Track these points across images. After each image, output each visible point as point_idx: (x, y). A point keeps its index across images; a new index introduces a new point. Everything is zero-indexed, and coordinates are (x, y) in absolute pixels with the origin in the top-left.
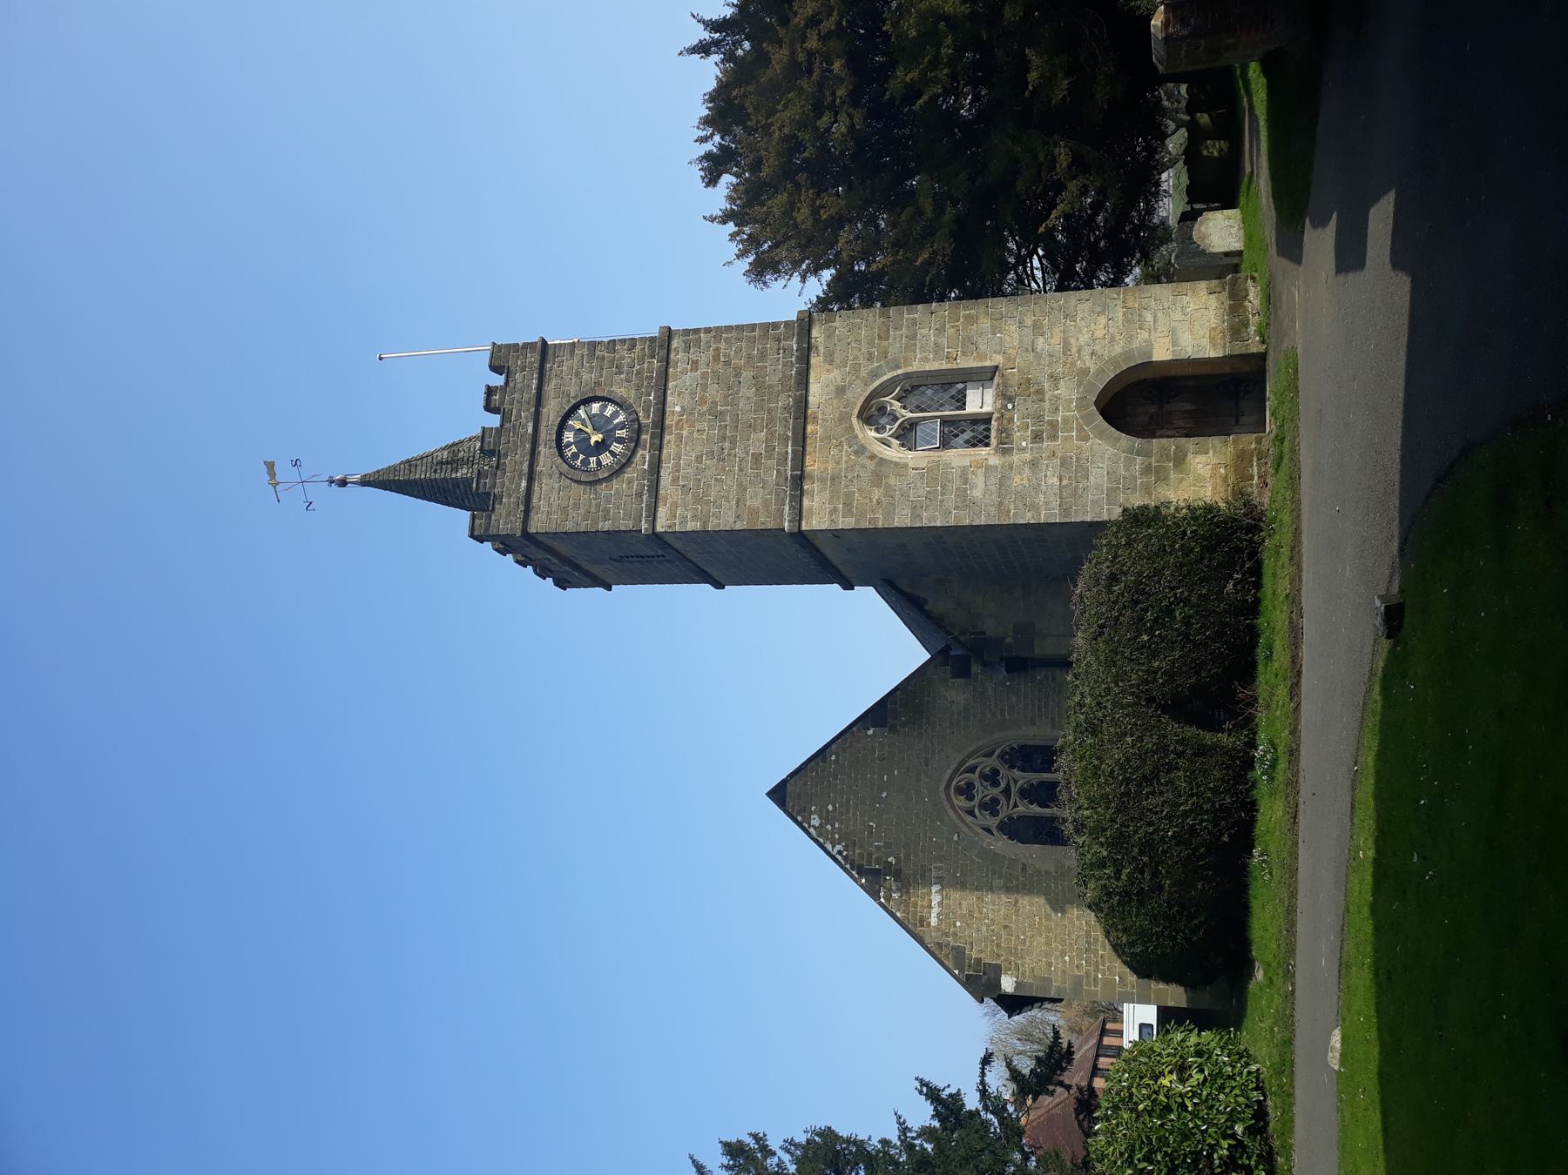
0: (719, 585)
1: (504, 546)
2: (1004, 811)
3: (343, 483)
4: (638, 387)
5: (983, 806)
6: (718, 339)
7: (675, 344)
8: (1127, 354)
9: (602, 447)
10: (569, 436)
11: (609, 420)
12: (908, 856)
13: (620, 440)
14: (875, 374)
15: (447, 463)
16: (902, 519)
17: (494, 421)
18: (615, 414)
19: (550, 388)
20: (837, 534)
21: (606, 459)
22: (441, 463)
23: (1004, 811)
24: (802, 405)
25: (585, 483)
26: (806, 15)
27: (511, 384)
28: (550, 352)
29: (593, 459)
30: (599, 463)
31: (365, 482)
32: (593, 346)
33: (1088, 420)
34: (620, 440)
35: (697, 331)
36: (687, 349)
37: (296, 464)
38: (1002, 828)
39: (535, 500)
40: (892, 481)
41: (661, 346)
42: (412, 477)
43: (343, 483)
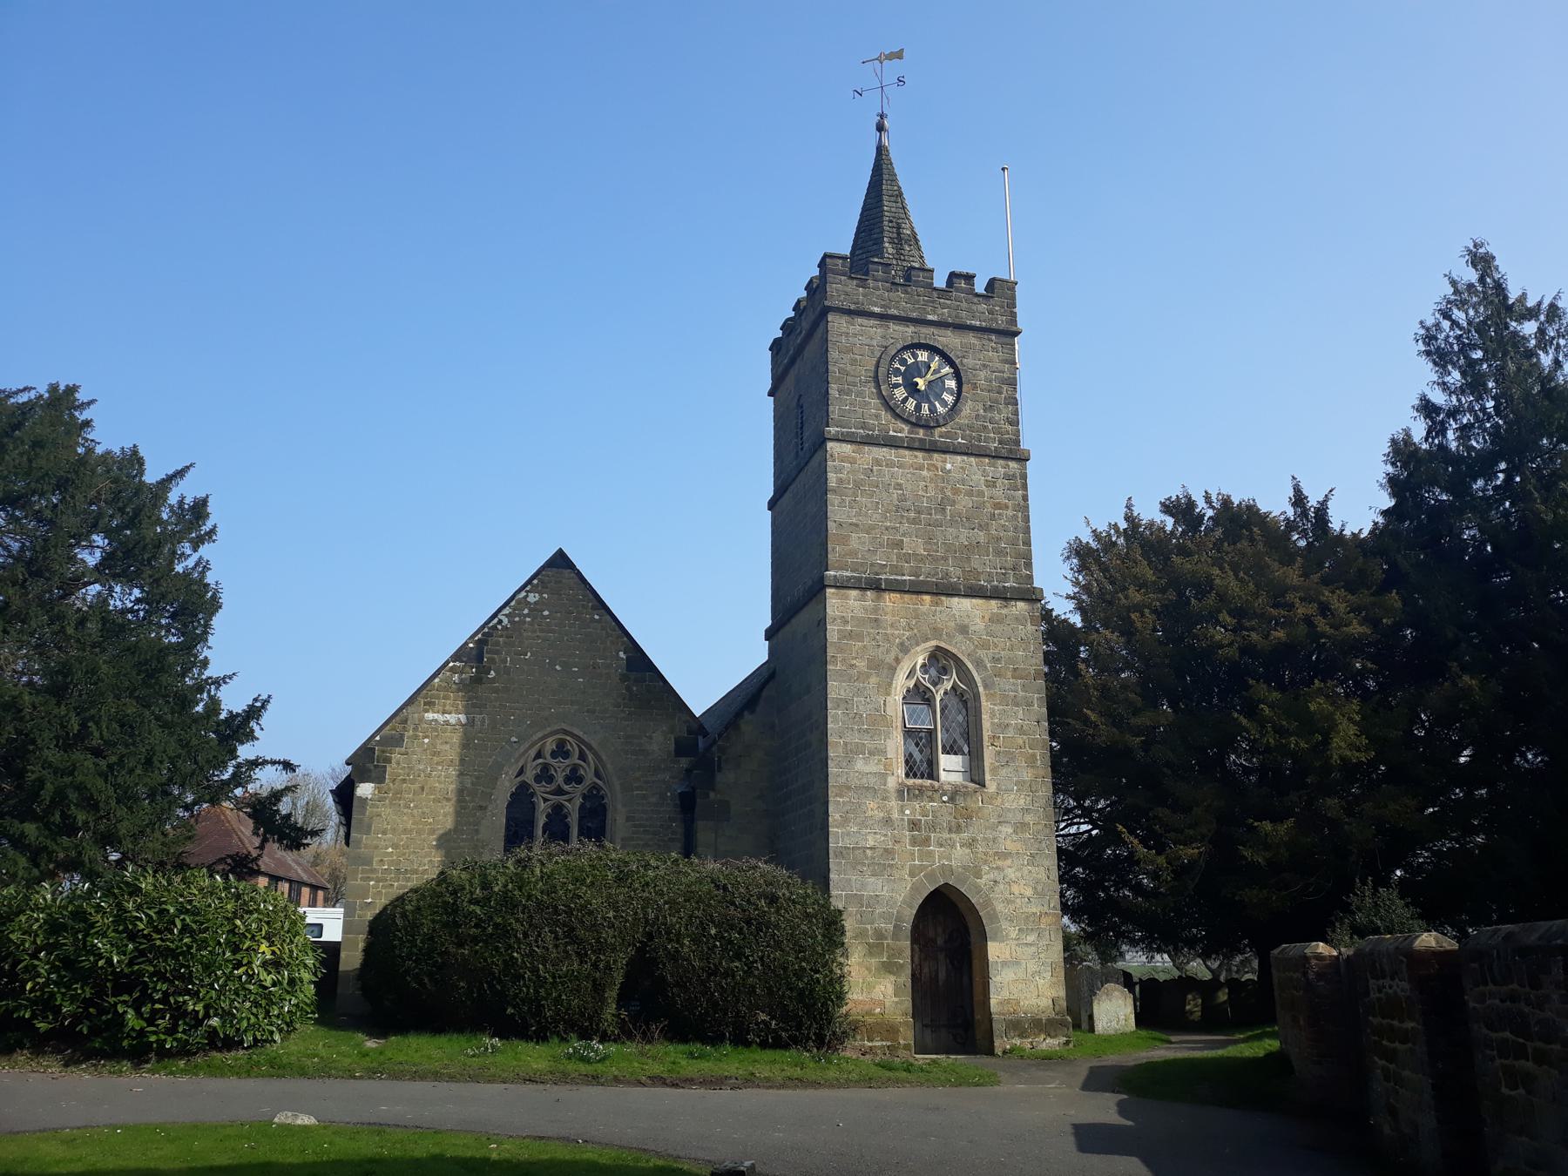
0: (772, 505)
1: (816, 289)
2: (539, 789)
3: (880, 128)
4: (971, 427)
5: (545, 767)
6: (1017, 508)
7: (1012, 464)
8: (994, 917)
9: (912, 389)
10: (923, 356)
11: (939, 397)
12: (496, 691)
13: (918, 408)
14: (979, 664)
15: (899, 234)
16: (835, 689)
17: (940, 281)
18: (944, 403)
19: (971, 339)
20: (822, 623)
21: (900, 393)
22: (899, 227)
23: (539, 789)
25: (876, 372)
27: (975, 300)
28: (1007, 340)
29: (900, 380)
30: (897, 386)
31: (881, 150)
32: (1012, 383)
33: (930, 876)
34: (918, 408)
35: (1025, 487)
36: (1007, 477)
37: (900, 80)
38: (523, 787)
40: (874, 680)
42: (885, 198)
43: (880, 128)
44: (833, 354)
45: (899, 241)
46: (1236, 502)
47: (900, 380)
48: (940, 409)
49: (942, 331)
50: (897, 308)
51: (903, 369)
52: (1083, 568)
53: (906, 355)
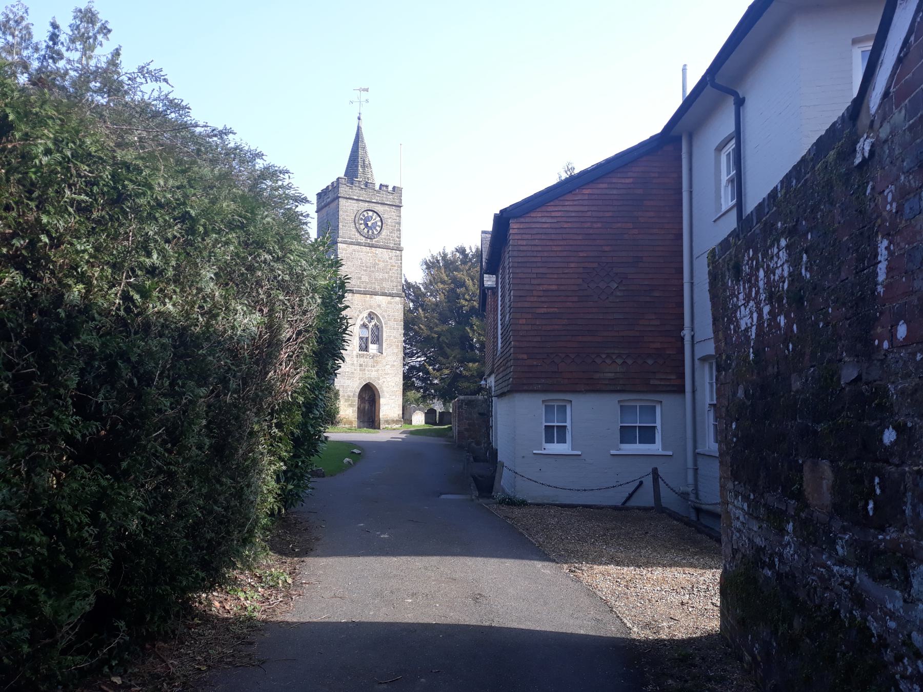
3: (359, 119)
7: (398, 252)
9: (366, 225)
10: (370, 213)
11: (375, 228)
13: (368, 232)
17: (377, 188)
18: (377, 230)
19: (386, 208)
21: (362, 227)
22: (364, 161)
24: (376, 294)
28: (398, 208)
29: (362, 222)
30: (361, 224)
31: (359, 128)
32: (399, 224)
34: (368, 232)
36: (396, 256)
39: (350, 201)
42: (360, 148)
43: (359, 119)
44: (341, 213)
45: (364, 166)
47: (362, 222)
48: (376, 232)
49: (377, 205)
53: (365, 213)
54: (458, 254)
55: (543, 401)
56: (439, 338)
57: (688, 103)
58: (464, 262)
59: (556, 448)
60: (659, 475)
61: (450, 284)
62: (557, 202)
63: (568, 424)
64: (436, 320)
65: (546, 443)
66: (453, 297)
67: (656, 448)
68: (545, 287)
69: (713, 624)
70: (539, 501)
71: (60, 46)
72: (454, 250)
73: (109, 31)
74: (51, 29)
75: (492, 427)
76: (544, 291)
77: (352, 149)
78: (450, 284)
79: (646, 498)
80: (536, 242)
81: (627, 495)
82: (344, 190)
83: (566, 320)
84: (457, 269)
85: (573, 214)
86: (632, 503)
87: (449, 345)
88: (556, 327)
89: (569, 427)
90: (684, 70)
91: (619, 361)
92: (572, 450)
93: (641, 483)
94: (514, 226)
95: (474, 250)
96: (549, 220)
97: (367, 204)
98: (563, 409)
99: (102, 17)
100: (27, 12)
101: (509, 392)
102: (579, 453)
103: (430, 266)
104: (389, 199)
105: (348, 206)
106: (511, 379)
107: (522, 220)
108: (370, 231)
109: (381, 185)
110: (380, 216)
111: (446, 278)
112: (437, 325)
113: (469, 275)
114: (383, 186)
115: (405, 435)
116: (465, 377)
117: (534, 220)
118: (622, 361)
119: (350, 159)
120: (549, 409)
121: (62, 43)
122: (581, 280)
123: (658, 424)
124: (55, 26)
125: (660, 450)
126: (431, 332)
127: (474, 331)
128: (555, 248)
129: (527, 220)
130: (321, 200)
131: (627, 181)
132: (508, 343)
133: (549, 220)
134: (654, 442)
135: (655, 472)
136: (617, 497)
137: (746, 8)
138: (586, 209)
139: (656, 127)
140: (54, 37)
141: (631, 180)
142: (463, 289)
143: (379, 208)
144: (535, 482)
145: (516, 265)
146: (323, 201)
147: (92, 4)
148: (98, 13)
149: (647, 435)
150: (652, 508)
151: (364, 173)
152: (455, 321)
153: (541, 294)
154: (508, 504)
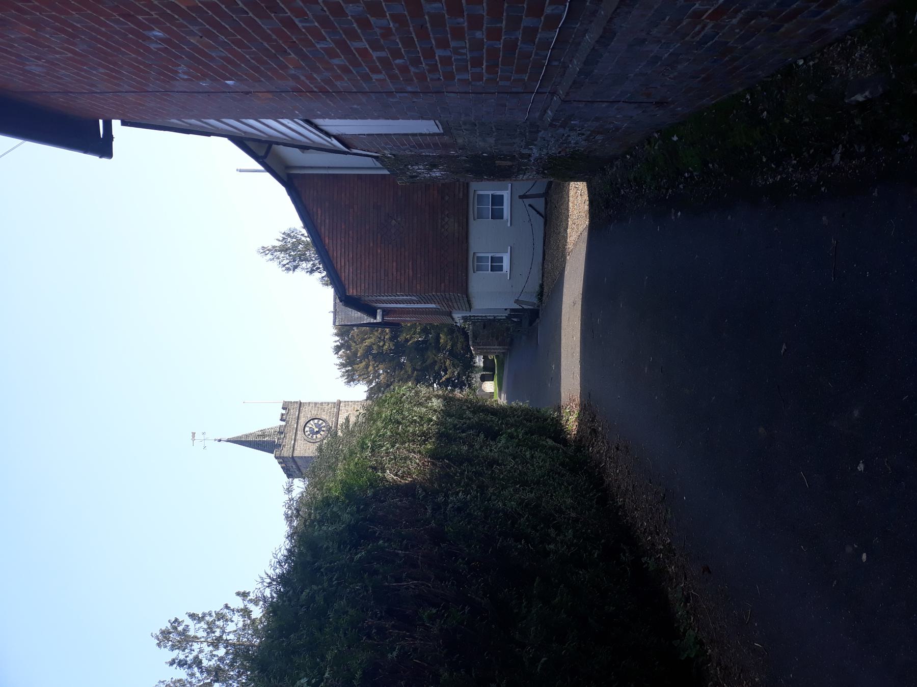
3: (220, 441)
4: (330, 416)
6: (354, 404)
7: (341, 405)
9: (318, 432)
10: (307, 429)
11: (320, 425)
13: (323, 431)
15: (261, 436)
17: (283, 423)
18: (322, 423)
19: (302, 415)
21: (319, 436)
22: (259, 436)
25: (312, 442)
26: (470, 468)
27: (289, 413)
28: (302, 405)
29: (315, 436)
30: (316, 437)
31: (229, 441)
32: (316, 404)
34: (323, 431)
35: (348, 402)
36: (345, 406)
37: (204, 433)
39: (296, 447)
41: (337, 405)
42: (247, 440)
43: (220, 441)
44: (306, 455)
45: (264, 435)
46: (336, 331)
47: (315, 436)
48: (324, 424)
49: (299, 423)
50: (292, 436)
51: (311, 435)
52: (353, 380)
53: (307, 434)
54: (340, 353)
55: (474, 272)
56: (417, 370)
57: (269, 169)
58: (348, 348)
59: (506, 264)
60: (523, 195)
61: (369, 360)
62: (334, 262)
63: (490, 255)
64: (402, 373)
65: (502, 271)
66: (380, 357)
67: (506, 195)
68: (394, 270)
69: (585, 183)
70: (541, 276)
71: (188, 659)
72: (336, 356)
73: (176, 620)
74: (175, 665)
75: (495, 317)
76: (397, 272)
77: (248, 447)
78: (369, 360)
79: (540, 203)
80: (363, 277)
81: (538, 215)
82: (286, 452)
83: (418, 256)
84: (355, 354)
85: (343, 250)
86: (542, 211)
87: (424, 361)
88: (422, 263)
89: (492, 255)
90: (241, 171)
91: (446, 219)
92: (507, 253)
93: (530, 205)
94: (352, 292)
95: (337, 338)
96: (347, 266)
97: (299, 432)
98: (480, 259)
99: (166, 625)
100: (163, 682)
101: (467, 296)
102: (509, 247)
103: (351, 378)
104: (294, 412)
105: (301, 449)
106: (459, 295)
107: (347, 286)
108: (323, 429)
109: (281, 420)
110: (310, 421)
111: (364, 363)
112: (406, 372)
113: (362, 342)
114: (282, 417)
115: (502, 394)
116: (452, 346)
117: (347, 278)
118: (446, 218)
119: (257, 449)
120: (479, 269)
121: (186, 657)
122: (390, 245)
123: (490, 193)
124: (172, 663)
125: (507, 191)
126: (412, 377)
127: (411, 338)
128: (367, 262)
129: (347, 282)
130: (293, 474)
131: (319, 212)
132: (433, 297)
133: (347, 266)
134: (503, 195)
135: (521, 197)
136: (541, 220)
137: (229, 141)
138: (339, 241)
139: (281, 190)
140: (182, 664)
141: (319, 209)
142: (375, 347)
143: (302, 421)
144: (528, 278)
145: (378, 291)
146: (295, 472)
147: (154, 634)
148: (161, 629)
149: (497, 200)
150: (546, 199)
151: (269, 436)
152: (401, 356)
153: (399, 273)
154: (542, 296)
